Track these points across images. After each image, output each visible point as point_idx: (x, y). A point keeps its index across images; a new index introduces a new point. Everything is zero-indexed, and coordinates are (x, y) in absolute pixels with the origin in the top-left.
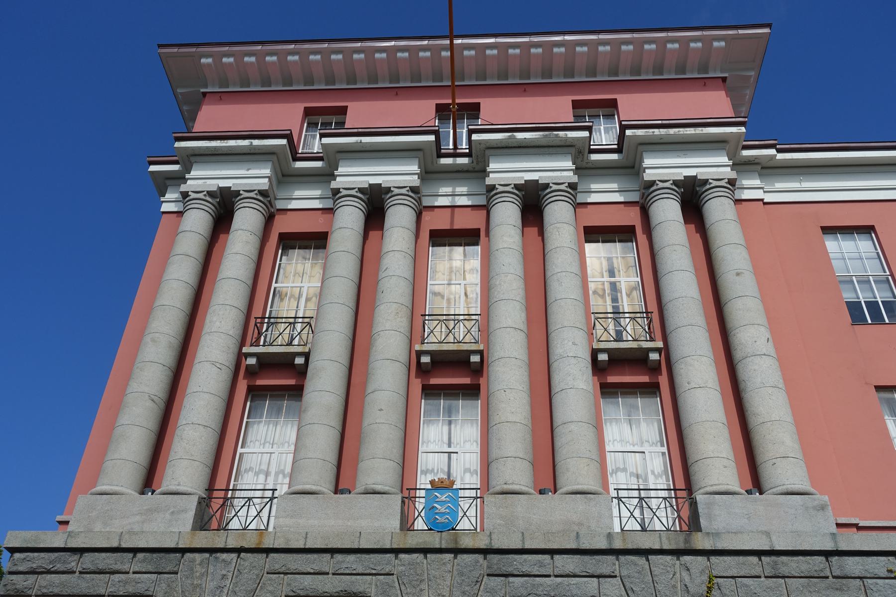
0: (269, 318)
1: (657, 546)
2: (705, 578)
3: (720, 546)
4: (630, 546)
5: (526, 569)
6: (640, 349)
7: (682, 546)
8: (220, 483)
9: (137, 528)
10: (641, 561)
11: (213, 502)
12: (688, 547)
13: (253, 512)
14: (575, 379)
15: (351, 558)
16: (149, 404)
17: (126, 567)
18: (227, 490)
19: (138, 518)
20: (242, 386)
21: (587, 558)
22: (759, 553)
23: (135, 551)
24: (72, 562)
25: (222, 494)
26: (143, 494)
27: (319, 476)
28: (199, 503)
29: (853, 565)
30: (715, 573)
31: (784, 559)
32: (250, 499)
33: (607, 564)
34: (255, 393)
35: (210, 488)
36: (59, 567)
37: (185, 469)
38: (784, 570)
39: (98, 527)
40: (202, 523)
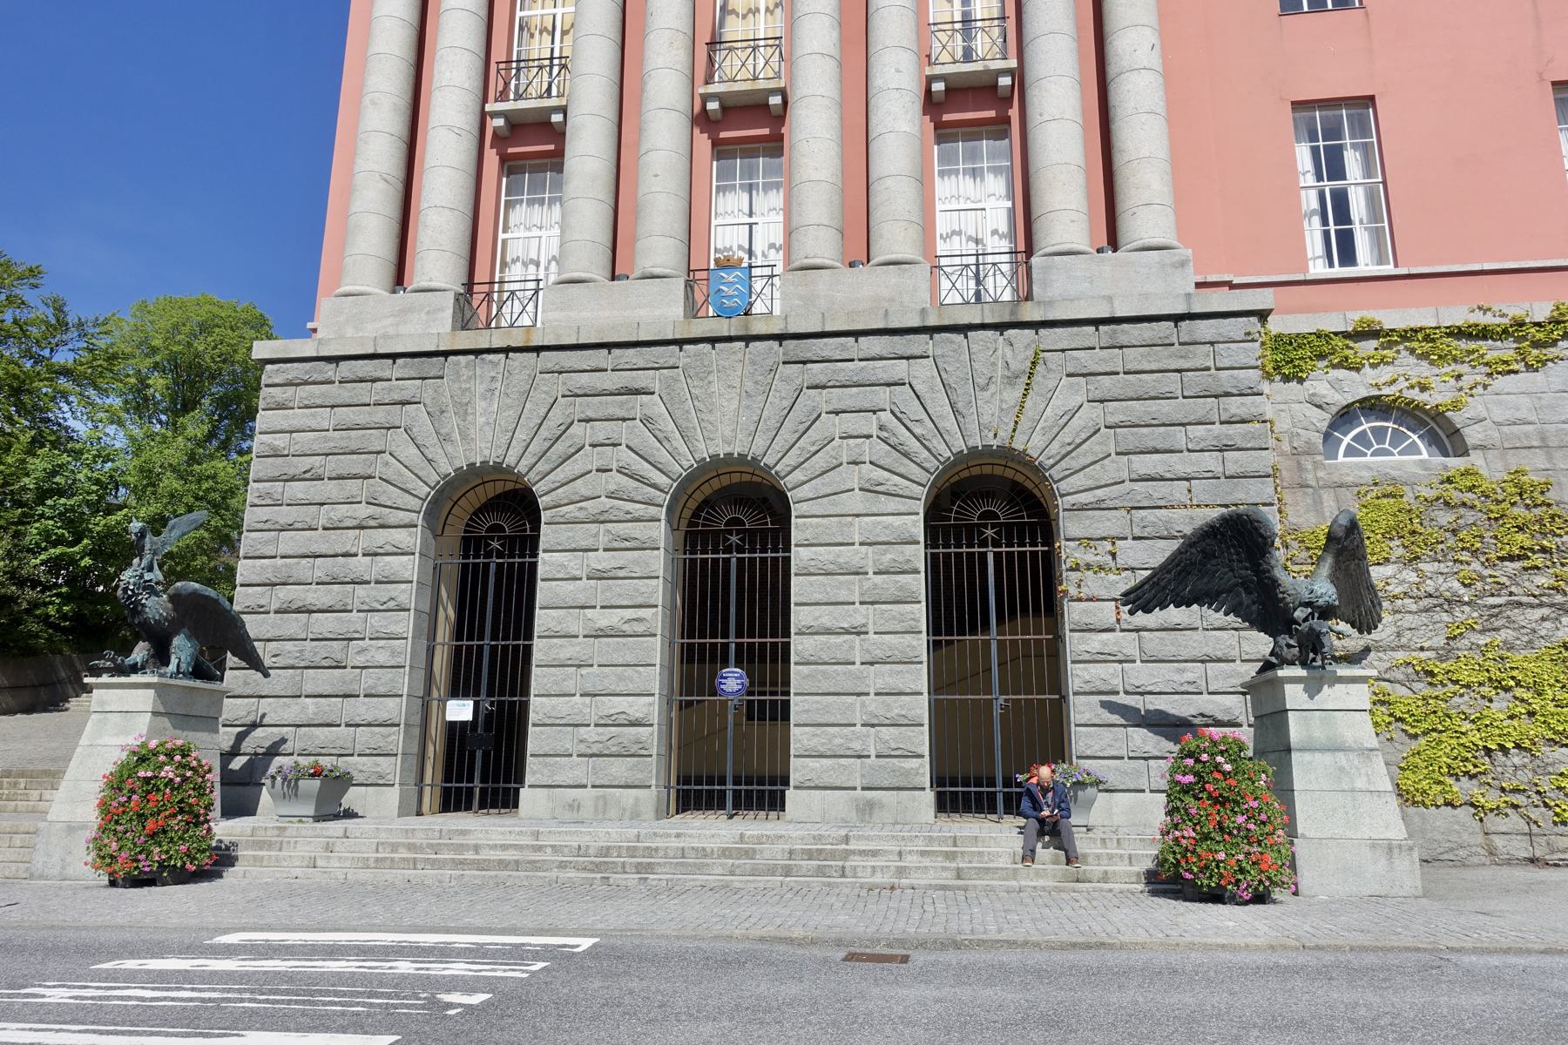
0: (518, 61)
1: (978, 321)
2: (1030, 353)
3: (1052, 316)
4: (946, 322)
5: (826, 354)
6: (987, 72)
7: (1006, 319)
8: (481, 275)
9: (391, 331)
10: (958, 338)
11: (474, 293)
12: (1014, 319)
13: (517, 307)
14: (899, 117)
15: (631, 351)
16: (382, 185)
17: (387, 374)
18: (492, 283)
19: (390, 320)
20: (492, 158)
21: (896, 338)
22: (1096, 322)
23: (394, 357)
24: (329, 370)
25: (486, 288)
26: (394, 292)
27: (589, 260)
28: (457, 300)
29: (1205, 329)
30: (1042, 347)
31: (1125, 326)
32: (513, 292)
33: (919, 343)
34: (511, 166)
35: (470, 284)
36: (315, 377)
37: (437, 262)
38: (1124, 340)
39: (350, 332)
40: (464, 320)
